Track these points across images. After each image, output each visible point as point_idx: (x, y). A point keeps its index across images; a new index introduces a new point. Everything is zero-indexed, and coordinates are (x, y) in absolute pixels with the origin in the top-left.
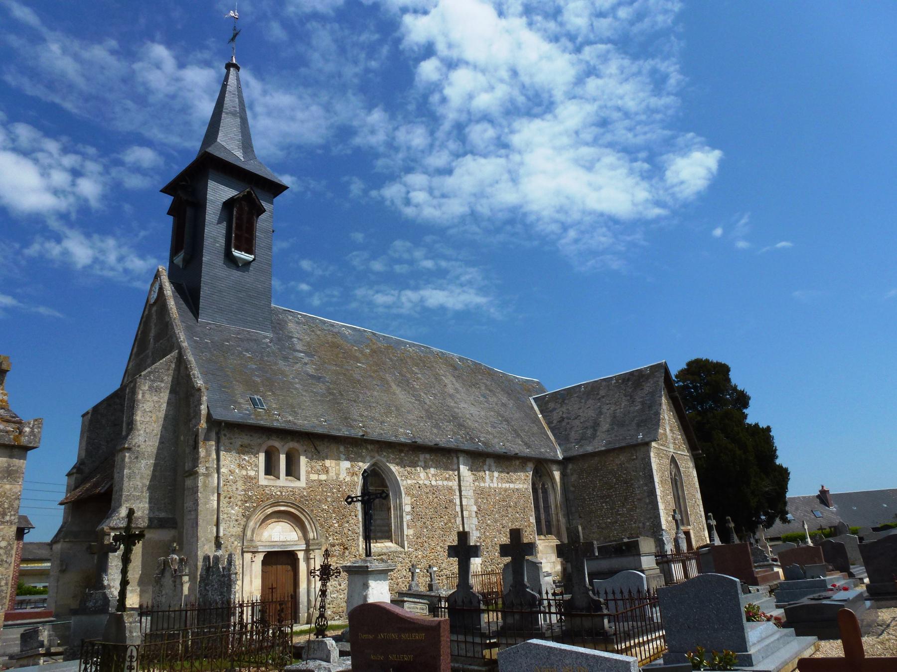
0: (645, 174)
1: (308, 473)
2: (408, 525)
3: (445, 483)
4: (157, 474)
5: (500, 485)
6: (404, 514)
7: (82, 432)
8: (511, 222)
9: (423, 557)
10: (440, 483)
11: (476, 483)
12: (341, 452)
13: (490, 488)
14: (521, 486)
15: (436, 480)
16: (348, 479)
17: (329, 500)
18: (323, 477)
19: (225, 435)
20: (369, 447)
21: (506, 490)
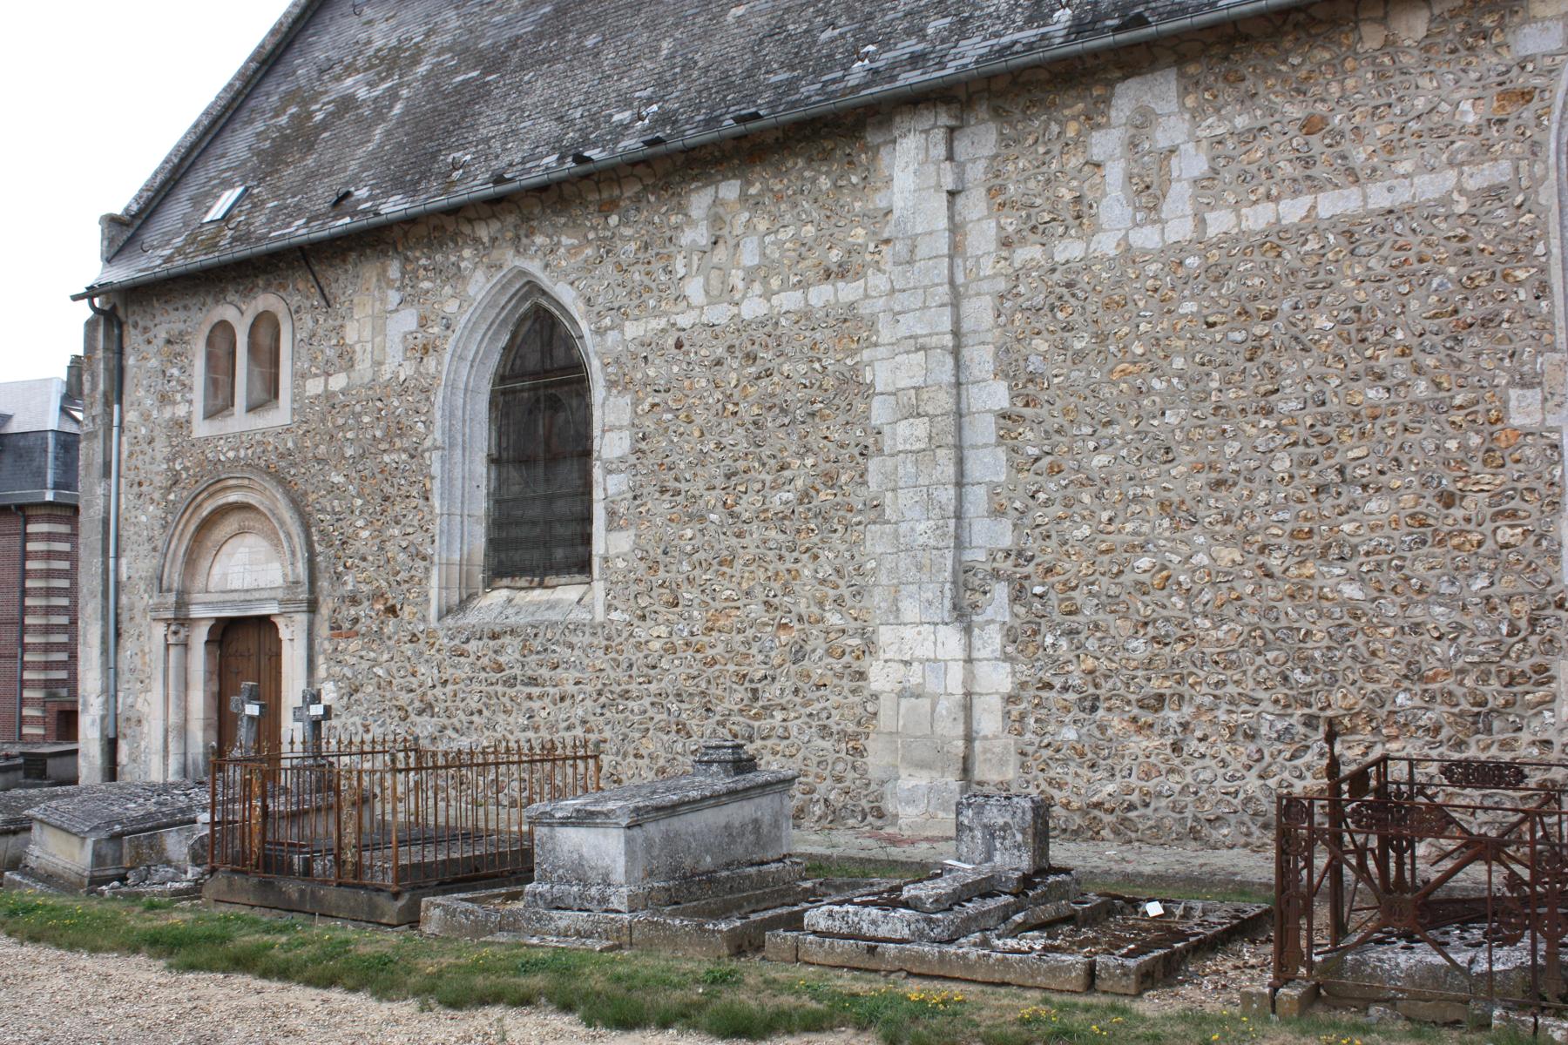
0: (220, 402)
1: (301, 376)
2: (611, 514)
3: (821, 295)
4: (32, 438)
5: (1220, 222)
6: (597, 473)
7: (146, 188)
8: (667, 174)
9: (671, 649)
10: (790, 300)
11: (1030, 253)
12: (390, 283)
13: (1129, 254)
14: (1429, 187)
15: (767, 295)
16: (407, 371)
17: (349, 452)
18: (338, 382)
19: (135, 325)
20: (483, 232)
21: (1274, 241)
